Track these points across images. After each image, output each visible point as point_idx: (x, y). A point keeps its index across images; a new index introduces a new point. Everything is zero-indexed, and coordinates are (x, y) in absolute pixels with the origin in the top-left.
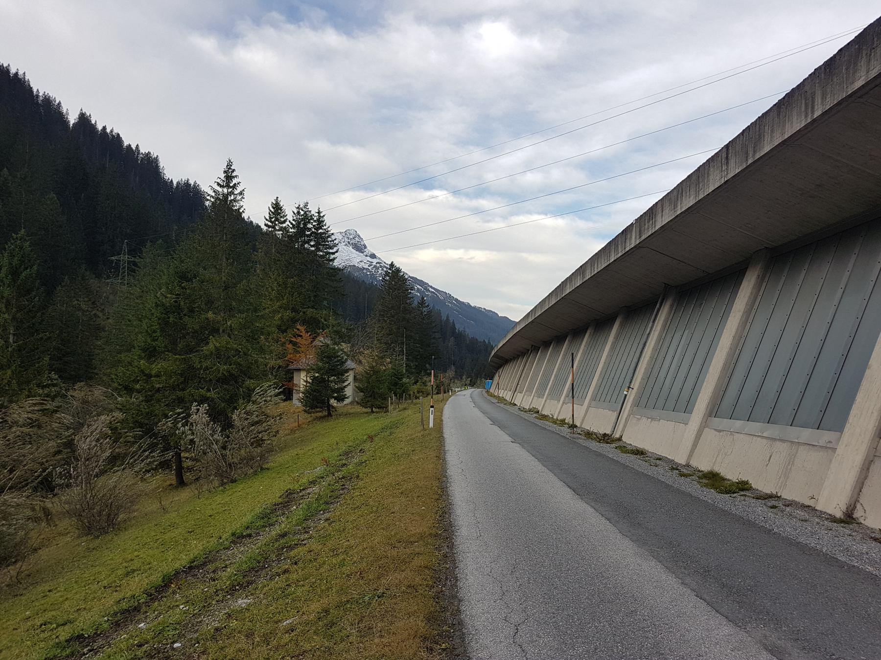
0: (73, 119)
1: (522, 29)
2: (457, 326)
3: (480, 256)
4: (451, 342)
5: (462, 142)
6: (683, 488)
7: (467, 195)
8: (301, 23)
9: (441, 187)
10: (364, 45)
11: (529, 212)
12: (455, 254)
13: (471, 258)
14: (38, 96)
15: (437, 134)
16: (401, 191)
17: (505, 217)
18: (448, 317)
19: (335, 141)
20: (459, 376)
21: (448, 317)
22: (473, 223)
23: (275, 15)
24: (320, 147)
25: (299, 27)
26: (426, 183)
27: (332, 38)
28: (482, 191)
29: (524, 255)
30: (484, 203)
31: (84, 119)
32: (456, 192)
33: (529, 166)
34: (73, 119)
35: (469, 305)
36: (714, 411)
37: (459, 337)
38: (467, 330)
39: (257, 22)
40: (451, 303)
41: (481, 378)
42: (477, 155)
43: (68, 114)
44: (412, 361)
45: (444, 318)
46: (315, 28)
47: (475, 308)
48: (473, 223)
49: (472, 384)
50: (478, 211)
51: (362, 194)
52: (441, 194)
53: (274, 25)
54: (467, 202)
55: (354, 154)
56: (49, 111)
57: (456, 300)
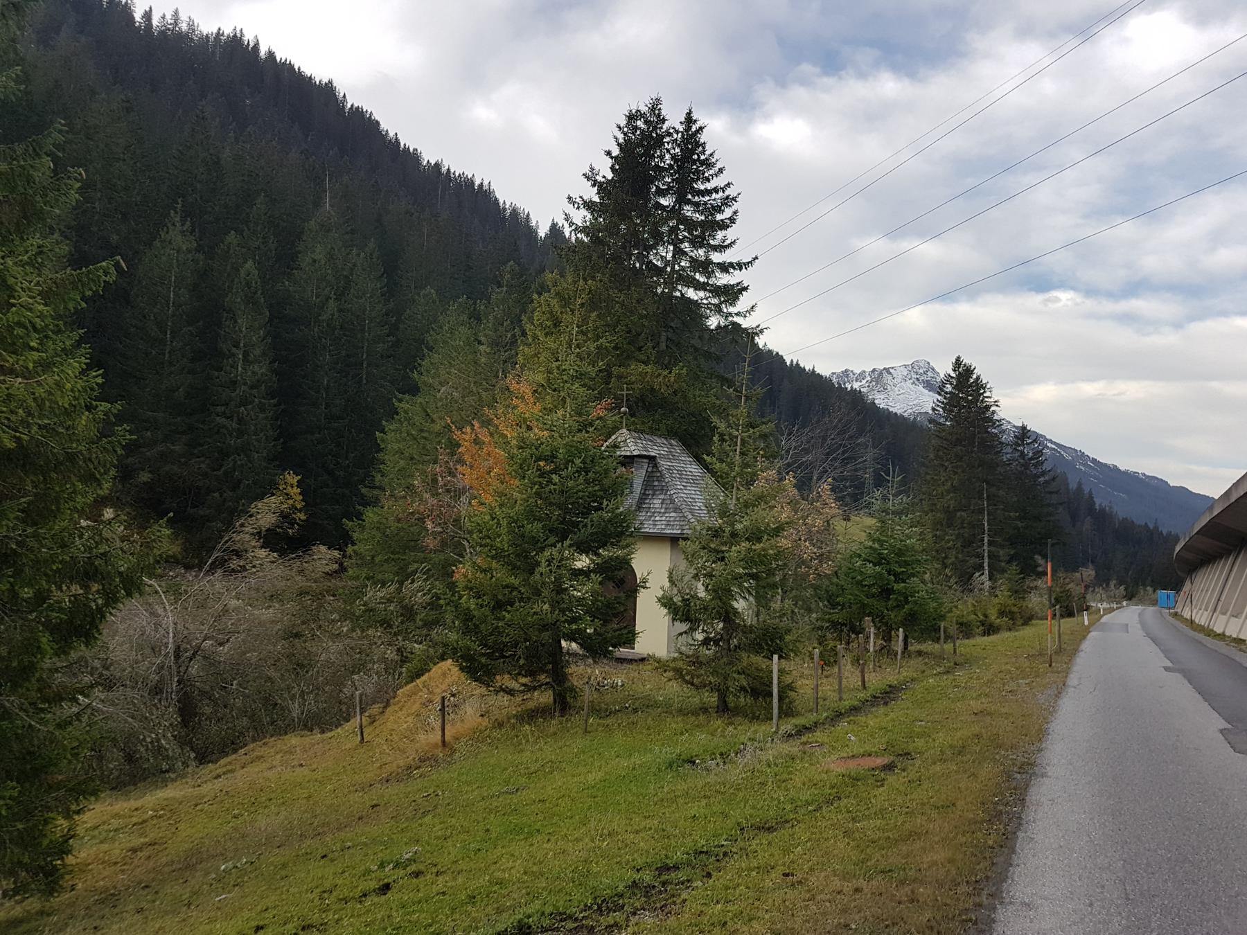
0: (543, 232)
1: (1202, 16)
2: (1097, 501)
3: (1133, 389)
4: (1087, 525)
5: (1098, 213)
6: (1237, 659)
7: (1111, 295)
8: (843, 73)
9: (1062, 285)
10: (939, 88)
11: (1225, 313)
12: (1090, 389)
13: (1118, 394)
14: (505, 209)
15: (1053, 207)
16: (1000, 298)
17: (1178, 325)
18: (1080, 484)
19: (895, 233)
20: (1102, 580)
21: (1080, 484)
22: (1122, 338)
23: (806, 68)
24: (875, 247)
25: (840, 78)
26: (1042, 284)
27: (889, 86)
28: (1137, 287)
29: (1215, 384)
30: (1138, 305)
31: (271, 55)
32: (1090, 291)
33: (1218, 237)
34: (543, 232)
35: (1116, 469)
36: (780, 717)
37: (1102, 518)
38: (1115, 509)
39: (782, 82)
40: (1086, 465)
41: (1145, 585)
42: (1126, 229)
43: (537, 226)
44: (1002, 546)
45: (1073, 486)
46: (862, 75)
47: (1126, 473)
48: (1122, 338)
49: (1130, 596)
50: (1128, 319)
51: (936, 307)
52: (1065, 297)
53: (805, 82)
54: (1109, 306)
55: (929, 250)
56: (412, 158)
57: (1094, 461)
